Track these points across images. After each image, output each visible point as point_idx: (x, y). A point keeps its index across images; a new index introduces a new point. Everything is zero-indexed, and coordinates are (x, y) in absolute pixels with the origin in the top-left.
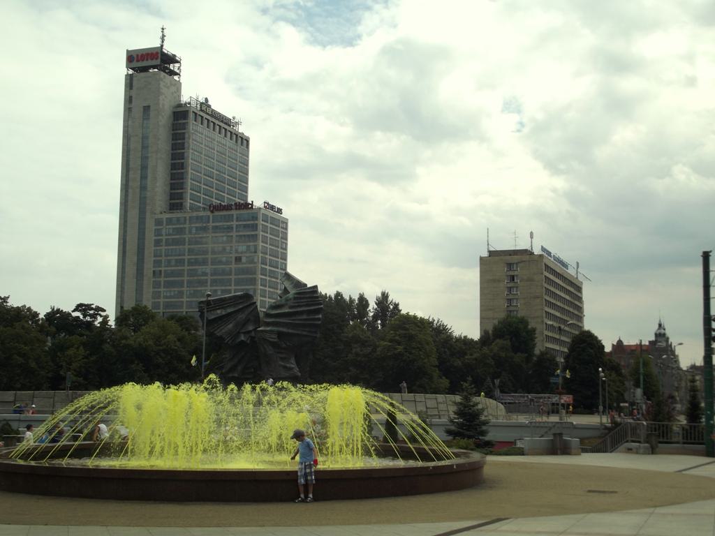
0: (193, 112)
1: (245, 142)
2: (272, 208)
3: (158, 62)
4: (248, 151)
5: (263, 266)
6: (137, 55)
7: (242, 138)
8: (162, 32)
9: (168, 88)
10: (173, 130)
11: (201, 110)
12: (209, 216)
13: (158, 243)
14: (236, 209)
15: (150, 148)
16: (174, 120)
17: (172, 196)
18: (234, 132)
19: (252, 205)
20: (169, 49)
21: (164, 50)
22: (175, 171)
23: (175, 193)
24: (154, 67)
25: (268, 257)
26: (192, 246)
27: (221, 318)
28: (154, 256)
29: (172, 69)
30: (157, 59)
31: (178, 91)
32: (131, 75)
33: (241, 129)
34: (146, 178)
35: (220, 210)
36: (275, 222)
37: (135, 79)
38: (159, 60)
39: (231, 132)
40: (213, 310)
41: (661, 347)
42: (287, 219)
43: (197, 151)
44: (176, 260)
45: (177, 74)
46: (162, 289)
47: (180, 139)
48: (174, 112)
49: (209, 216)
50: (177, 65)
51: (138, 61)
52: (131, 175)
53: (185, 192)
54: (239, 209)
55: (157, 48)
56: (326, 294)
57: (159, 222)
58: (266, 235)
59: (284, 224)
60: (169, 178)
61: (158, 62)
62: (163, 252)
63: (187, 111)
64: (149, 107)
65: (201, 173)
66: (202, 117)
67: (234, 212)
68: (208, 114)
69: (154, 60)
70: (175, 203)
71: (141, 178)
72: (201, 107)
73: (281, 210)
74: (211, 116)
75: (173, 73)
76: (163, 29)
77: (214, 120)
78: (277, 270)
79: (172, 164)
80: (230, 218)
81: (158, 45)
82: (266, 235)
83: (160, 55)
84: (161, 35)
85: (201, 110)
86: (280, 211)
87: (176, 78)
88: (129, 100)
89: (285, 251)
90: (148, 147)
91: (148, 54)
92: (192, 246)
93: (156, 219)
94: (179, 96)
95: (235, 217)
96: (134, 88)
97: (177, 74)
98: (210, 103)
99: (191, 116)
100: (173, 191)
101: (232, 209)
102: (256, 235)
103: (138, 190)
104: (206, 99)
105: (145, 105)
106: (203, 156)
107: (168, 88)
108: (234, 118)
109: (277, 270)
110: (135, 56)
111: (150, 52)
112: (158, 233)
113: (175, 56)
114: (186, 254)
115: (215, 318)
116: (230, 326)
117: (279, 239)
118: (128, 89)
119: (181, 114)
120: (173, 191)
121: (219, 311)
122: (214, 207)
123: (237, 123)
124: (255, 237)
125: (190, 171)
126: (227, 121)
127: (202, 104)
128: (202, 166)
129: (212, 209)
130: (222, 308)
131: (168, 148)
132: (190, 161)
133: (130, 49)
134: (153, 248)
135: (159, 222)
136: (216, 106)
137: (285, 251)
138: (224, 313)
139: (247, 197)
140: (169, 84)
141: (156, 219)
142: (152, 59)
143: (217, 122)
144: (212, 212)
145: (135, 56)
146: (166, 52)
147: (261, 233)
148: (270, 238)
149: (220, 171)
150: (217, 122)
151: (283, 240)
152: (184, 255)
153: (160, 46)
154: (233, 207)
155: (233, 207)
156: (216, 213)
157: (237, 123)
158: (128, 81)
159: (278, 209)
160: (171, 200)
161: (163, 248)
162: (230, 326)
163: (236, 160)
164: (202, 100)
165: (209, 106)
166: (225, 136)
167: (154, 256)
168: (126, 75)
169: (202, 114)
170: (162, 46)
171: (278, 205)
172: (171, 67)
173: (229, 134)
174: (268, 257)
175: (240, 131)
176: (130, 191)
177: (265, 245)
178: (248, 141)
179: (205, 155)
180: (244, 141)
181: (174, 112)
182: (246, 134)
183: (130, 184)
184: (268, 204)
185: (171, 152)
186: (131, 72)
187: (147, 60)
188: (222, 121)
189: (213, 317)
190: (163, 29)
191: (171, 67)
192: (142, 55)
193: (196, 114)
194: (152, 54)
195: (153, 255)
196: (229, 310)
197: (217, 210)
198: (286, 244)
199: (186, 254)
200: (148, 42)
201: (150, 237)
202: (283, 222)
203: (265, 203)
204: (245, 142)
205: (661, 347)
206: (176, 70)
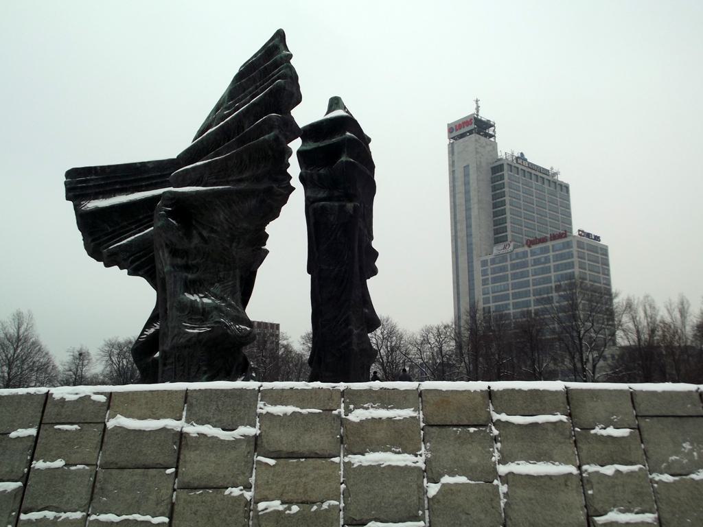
2: (588, 235)
3: (473, 126)
4: (569, 196)
6: (456, 126)
8: (477, 104)
9: (484, 147)
10: (492, 183)
12: (527, 251)
13: (485, 282)
14: (551, 240)
15: (471, 201)
17: (496, 232)
20: (484, 115)
26: (514, 262)
28: (483, 294)
30: (471, 124)
33: (561, 178)
34: (471, 226)
35: (537, 244)
36: (594, 249)
42: (607, 246)
43: (514, 198)
46: (490, 286)
50: (492, 128)
51: (457, 130)
58: (583, 261)
59: (604, 251)
60: (492, 225)
62: (490, 289)
63: (503, 164)
64: (468, 166)
67: (549, 244)
70: (499, 236)
71: (467, 227)
73: (599, 237)
76: (477, 101)
77: (530, 170)
79: (494, 212)
80: (546, 250)
82: (583, 261)
83: (473, 121)
86: (597, 238)
87: (492, 139)
88: (452, 164)
89: (607, 277)
90: (470, 200)
92: (514, 262)
93: (482, 262)
95: (551, 248)
96: (455, 154)
98: (526, 157)
99: (506, 167)
100: (496, 236)
103: (465, 238)
104: (522, 154)
105: (465, 165)
106: (521, 202)
107: (484, 147)
108: (552, 168)
111: (465, 120)
112: (484, 273)
113: (489, 121)
114: (510, 289)
118: (451, 156)
119: (497, 169)
120: (496, 236)
126: (546, 172)
127: (517, 158)
131: (489, 198)
133: (450, 123)
134: (481, 278)
136: (532, 158)
140: (484, 144)
141: (482, 262)
143: (533, 172)
144: (529, 246)
145: (454, 128)
148: (588, 254)
150: (533, 172)
152: (508, 290)
154: (549, 239)
155: (549, 239)
157: (555, 174)
159: (595, 237)
161: (490, 286)
164: (517, 154)
165: (526, 160)
167: (483, 294)
168: (449, 145)
169: (517, 165)
171: (594, 233)
174: (587, 272)
175: (559, 179)
176: (459, 240)
179: (523, 201)
180: (565, 188)
182: (566, 181)
183: (459, 234)
184: (583, 231)
185: (492, 202)
190: (477, 101)
192: (460, 125)
194: (467, 122)
195: (481, 294)
197: (533, 244)
198: (609, 270)
199: (510, 289)
200: (464, 111)
201: (478, 278)
202: (602, 249)
203: (579, 231)
206: (491, 132)
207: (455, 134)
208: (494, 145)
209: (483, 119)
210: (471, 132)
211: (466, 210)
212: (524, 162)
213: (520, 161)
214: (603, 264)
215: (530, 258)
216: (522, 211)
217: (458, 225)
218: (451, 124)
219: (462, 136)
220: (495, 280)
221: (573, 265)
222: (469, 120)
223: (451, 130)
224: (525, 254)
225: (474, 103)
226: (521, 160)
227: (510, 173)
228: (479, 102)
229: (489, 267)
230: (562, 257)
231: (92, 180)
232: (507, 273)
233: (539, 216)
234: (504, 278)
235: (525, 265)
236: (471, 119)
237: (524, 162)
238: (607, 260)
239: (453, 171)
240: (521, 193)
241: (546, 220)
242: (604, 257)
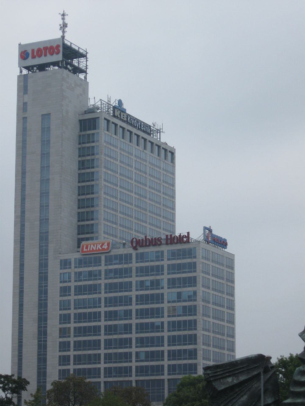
0: (105, 119)
1: (169, 155)
3: (59, 57)
4: (174, 167)
5: (205, 318)
6: (33, 51)
7: (166, 150)
8: (63, 19)
11: (114, 116)
12: (131, 255)
13: (65, 291)
14: (167, 244)
16: (81, 131)
18: (155, 142)
19: (188, 237)
21: (66, 42)
22: (83, 197)
23: (83, 226)
24: (55, 64)
25: (211, 306)
27: (232, 388)
29: (76, 65)
30: (58, 53)
31: (25, 104)
32: (25, 76)
33: (165, 138)
35: (146, 246)
37: (30, 81)
38: (61, 55)
39: (152, 143)
40: (222, 378)
41: (9, 397)
44: (184, 308)
45: (82, 71)
47: (88, 155)
48: (80, 121)
49: (131, 255)
50: (82, 60)
51: (33, 57)
52: (28, 205)
53: (97, 224)
54: (171, 243)
55: (59, 39)
56: (291, 355)
57: (65, 264)
60: (76, 207)
61: (59, 57)
65: (116, 198)
66: (116, 125)
67: (165, 249)
68: (123, 121)
69: (55, 55)
72: (114, 112)
74: (127, 122)
75: (77, 70)
76: (63, 15)
78: (222, 323)
81: (58, 35)
83: (61, 49)
84: (61, 22)
85: (114, 116)
86: (223, 243)
87: (82, 76)
91: (46, 48)
94: (87, 99)
97: (82, 71)
98: (125, 106)
99: (102, 124)
101: (161, 244)
102: (195, 278)
104: (120, 102)
105: (45, 113)
109: (222, 323)
110: (30, 52)
115: (226, 389)
116: (245, 398)
117: (224, 282)
118: (22, 94)
121: (230, 380)
122: (138, 242)
123: (159, 131)
124: (192, 281)
125: (103, 196)
126: (146, 129)
127: (114, 107)
128: (118, 188)
129: (134, 245)
130: (234, 375)
131: (74, 166)
132: (103, 183)
135: (65, 264)
137: (231, 298)
138: (235, 382)
139: (174, 226)
140: (73, 85)
141: (61, 261)
142: (52, 54)
144: (135, 248)
145: (30, 52)
146: (69, 44)
147: (202, 275)
149: (140, 195)
150: (134, 130)
151: (229, 284)
153: (60, 37)
154: (164, 242)
155: (164, 242)
156: (141, 250)
157: (159, 131)
158: (22, 83)
160: (79, 234)
162: (245, 398)
163: (160, 179)
164: (113, 103)
165: (124, 111)
166: (145, 148)
170: (63, 37)
172: (75, 62)
173: (149, 145)
174: (211, 306)
176: (27, 224)
177: (207, 290)
178: (173, 154)
179: (121, 174)
181: (80, 121)
182: (171, 144)
183: (27, 215)
186: (25, 72)
187: (45, 55)
188: (140, 129)
189: (223, 387)
190: (63, 15)
191: (75, 62)
192: (39, 50)
193: (108, 121)
194: (52, 47)
196: (242, 378)
197: (142, 246)
198: (233, 288)
204: (169, 155)
205: (9, 397)
206: (82, 66)
207: (30, 62)
208: (84, 85)
209: (73, 46)
210: (55, 64)
211: (42, 181)
212: (122, 114)
213: (117, 113)
214: (228, 280)
215: (134, 265)
216: (118, 188)
217: (27, 201)
218: (26, 45)
219: (42, 67)
220: (80, 290)
221: (195, 282)
222: (55, 46)
223: (24, 55)
224: (127, 258)
225: (61, 17)
226: (119, 112)
227: (107, 132)
228: (66, 17)
229: (73, 270)
230: (179, 268)
231: (219, 371)
232: (99, 282)
233: (137, 197)
234: (94, 289)
235: (127, 272)
236: (58, 46)
237: (122, 114)
238: (233, 274)
239: (25, 118)
240: (133, 170)
241: (146, 203)
242: (229, 270)
